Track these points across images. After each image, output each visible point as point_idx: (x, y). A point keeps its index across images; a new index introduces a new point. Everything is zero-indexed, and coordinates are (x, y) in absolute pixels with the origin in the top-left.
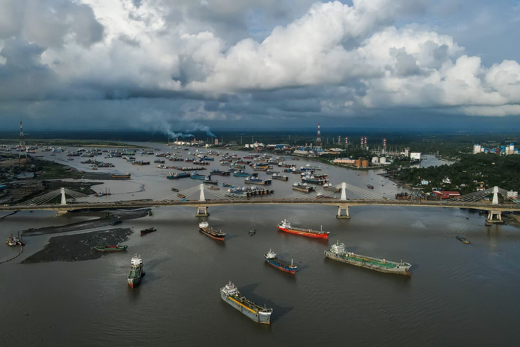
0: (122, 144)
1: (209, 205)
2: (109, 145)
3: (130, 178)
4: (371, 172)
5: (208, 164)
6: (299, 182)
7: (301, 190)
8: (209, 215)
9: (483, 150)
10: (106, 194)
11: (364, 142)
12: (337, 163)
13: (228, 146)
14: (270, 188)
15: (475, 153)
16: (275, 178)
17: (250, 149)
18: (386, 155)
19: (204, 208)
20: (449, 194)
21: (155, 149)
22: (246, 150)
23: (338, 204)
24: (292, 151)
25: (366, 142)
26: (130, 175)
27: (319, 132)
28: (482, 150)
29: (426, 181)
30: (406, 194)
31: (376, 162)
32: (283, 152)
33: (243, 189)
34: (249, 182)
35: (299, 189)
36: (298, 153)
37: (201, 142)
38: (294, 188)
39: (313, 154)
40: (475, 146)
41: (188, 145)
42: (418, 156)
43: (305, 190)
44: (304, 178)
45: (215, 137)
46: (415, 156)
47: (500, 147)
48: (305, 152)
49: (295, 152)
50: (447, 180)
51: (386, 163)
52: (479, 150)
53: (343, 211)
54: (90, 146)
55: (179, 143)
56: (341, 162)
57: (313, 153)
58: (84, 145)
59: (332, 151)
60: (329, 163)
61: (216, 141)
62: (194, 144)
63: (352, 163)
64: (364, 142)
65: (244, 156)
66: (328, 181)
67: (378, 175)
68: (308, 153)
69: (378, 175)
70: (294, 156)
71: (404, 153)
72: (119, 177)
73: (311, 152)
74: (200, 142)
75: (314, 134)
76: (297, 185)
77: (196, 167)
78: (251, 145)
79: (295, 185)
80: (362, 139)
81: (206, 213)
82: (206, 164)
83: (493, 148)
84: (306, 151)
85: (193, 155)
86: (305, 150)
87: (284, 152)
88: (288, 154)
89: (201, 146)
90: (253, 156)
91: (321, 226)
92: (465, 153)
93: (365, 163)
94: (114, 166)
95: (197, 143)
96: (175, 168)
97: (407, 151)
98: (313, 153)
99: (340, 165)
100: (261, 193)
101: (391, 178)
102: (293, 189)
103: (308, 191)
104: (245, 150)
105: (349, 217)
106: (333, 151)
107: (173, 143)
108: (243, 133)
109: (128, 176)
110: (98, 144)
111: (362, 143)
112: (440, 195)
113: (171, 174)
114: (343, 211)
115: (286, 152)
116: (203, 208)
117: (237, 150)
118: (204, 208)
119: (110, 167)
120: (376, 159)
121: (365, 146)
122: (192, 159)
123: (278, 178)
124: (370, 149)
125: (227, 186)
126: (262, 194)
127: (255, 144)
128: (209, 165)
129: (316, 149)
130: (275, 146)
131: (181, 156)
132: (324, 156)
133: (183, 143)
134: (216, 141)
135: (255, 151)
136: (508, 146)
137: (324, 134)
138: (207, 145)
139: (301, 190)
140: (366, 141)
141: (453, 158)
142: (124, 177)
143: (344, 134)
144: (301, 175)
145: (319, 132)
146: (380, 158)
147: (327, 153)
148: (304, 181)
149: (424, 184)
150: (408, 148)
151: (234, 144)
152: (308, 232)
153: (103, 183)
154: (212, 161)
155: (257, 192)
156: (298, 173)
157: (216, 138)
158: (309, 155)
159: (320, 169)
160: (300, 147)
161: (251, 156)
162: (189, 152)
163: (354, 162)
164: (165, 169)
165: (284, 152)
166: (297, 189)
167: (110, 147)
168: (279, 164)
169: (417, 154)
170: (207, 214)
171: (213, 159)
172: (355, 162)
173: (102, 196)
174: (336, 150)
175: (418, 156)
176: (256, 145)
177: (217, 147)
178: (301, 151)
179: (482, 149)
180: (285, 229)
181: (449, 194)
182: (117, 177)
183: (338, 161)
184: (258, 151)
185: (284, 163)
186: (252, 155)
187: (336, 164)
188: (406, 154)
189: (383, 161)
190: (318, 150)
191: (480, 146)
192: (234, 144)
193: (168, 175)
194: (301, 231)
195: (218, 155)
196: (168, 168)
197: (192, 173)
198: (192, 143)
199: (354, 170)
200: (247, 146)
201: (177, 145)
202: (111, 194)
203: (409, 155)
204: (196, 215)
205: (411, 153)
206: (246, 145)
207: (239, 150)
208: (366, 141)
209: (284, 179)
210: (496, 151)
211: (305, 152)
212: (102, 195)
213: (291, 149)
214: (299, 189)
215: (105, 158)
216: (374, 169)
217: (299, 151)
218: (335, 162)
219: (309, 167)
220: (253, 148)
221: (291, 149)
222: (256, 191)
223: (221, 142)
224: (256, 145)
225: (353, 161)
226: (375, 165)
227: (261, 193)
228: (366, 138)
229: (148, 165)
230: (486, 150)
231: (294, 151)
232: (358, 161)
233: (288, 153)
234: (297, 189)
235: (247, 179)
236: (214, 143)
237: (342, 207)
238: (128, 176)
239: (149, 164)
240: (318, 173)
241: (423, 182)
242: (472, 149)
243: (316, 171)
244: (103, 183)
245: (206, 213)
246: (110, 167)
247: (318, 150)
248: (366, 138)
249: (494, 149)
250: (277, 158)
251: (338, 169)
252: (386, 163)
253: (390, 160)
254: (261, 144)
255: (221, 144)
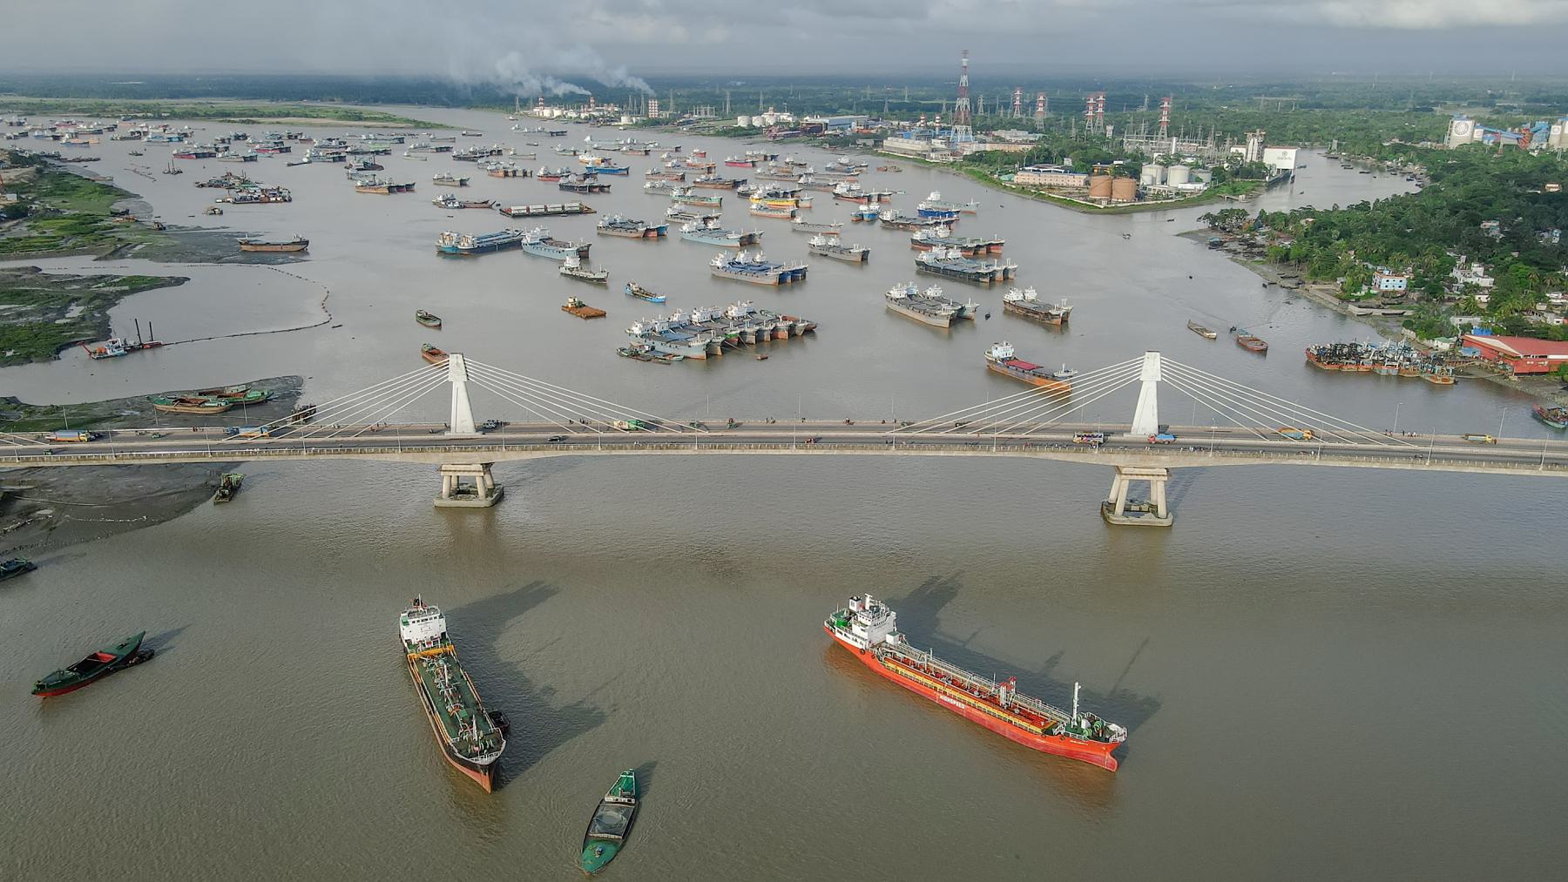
0: (378, 113)
1: (497, 457)
2: (340, 118)
3: (308, 254)
4: (1142, 224)
5: (606, 189)
6: (911, 283)
7: (917, 316)
8: (500, 498)
9: (1478, 134)
10: (141, 344)
11: (1095, 109)
12: (1029, 184)
13: (688, 122)
14: (797, 306)
15: (1453, 146)
16: (823, 254)
17: (750, 132)
18: (1185, 157)
19: (473, 467)
20: (1550, 357)
21: (464, 132)
22: (739, 135)
23: (1117, 459)
24: (878, 140)
25: (1100, 110)
26: (307, 243)
27: (964, 79)
28: (1475, 136)
29: (1398, 279)
30: (1354, 353)
31: (1154, 179)
32: (849, 142)
33: (695, 318)
34: (727, 275)
35: (910, 313)
36: (895, 148)
37: (610, 109)
38: (894, 306)
39: (942, 150)
40: (1456, 122)
41: (571, 117)
42: (1289, 158)
43: (933, 321)
44: (925, 257)
45: (651, 92)
46: (1279, 158)
47: (1533, 125)
48: (919, 146)
49: (886, 143)
50: (1474, 269)
51: (1189, 186)
52: (1468, 134)
53: (1139, 489)
54: (278, 123)
55: (547, 113)
56: (1037, 183)
57: (943, 146)
58: (261, 120)
59: (1001, 140)
60: (998, 184)
61: (653, 106)
62: (587, 115)
63: (1077, 184)
64: (1095, 109)
65: (729, 159)
66: (1015, 270)
67: (1178, 235)
68: (927, 148)
69: (1178, 235)
70: (885, 155)
71: (1242, 150)
72: (264, 248)
73: (937, 143)
74: (607, 111)
75: (954, 92)
76: (903, 296)
77: (560, 205)
78: (754, 118)
79: (895, 293)
80: (1092, 101)
81: (481, 492)
82: (597, 190)
83: (1510, 129)
84: (922, 143)
85: (572, 153)
86: (918, 138)
87: (854, 143)
88: (866, 150)
89: (609, 121)
90: (756, 156)
91: (1077, 687)
92: (1409, 144)
93: (1124, 186)
94: (290, 200)
95: (595, 114)
96: (490, 207)
97: (1253, 143)
98: (943, 146)
99: (1039, 194)
100: (767, 337)
101: (1235, 252)
102: (889, 312)
103: (946, 323)
104: (735, 136)
105: (1167, 523)
106: (1009, 142)
107: (529, 112)
108: (739, 81)
109: (300, 247)
110: (306, 116)
111: (1091, 113)
112: (1508, 357)
113: (451, 241)
114: (1139, 489)
115: (858, 143)
116: (467, 466)
117: (712, 135)
118: (473, 467)
119: (273, 202)
120: (1154, 170)
121: (1097, 122)
122: (559, 171)
123: (830, 254)
124: (1118, 132)
125: (640, 297)
126: (766, 342)
127: (765, 115)
128: (609, 192)
129: (953, 132)
130: (827, 121)
131: (533, 157)
132: (978, 158)
133: (557, 113)
134: (653, 106)
135: (765, 139)
136: (1559, 121)
137: (972, 91)
138: (624, 120)
139: (917, 316)
140: (1165, 112)
141: (1389, 163)
142: (285, 249)
143: (1032, 86)
144: (912, 240)
145: (964, 79)
146: (1170, 168)
147: (988, 147)
148: (926, 270)
149: (1390, 288)
150: (1258, 133)
151: (706, 114)
152: (993, 700)
153: (179, 281)
154: (623, 178)
155: (750, 334)
156: (899, 229)
157: (652, 98)
158: (933, 155)
159: (973, 210)
160: (902, 123)
161: (751, 157)
162: (559, 145)
163: (1082, 184)
164: (456, 210)
165: (854, 143)
166: (903, 310)
167: (336, 126)
168: (838, 190)
169: (1285, 154)
170: (489, 492)
171: (627, 169)
172: (1087, 183)
173: (122, 355)
174: (1017, 141)
175: (1289, 158)
176: (769, 118)
177: (655, 123)
178: (906, 140)
179: (1476, 130)
180: (863, 652)
181: (1550, 357)
182: (259, 249)
183: (1026, 177)
184: (776, 140)
185: (854, 187)
186: (755, 153)
187: (1023, 190)
188: (1250, 152)
189: (1178, 178)
190: (961, 138)
191: (1470, 123)
192: (706, 114)
193: (441, 241)
194: (954, 682)
195: (647, 152)
196: (465, 207)
197: (531, 232)
198: (584, 112)
199: (1091, 213)
200: (742, 121)
201: (539, 117)
202: (159, 345)
203: (1260, 155)
204: (437, 503)
205: (1266, 150)
206: (739, 118)
207: (718, 134)
208: (1041, 104)
209: (853, 259)
210: (1517, 139)
211: (919, 146)
212: (122, 351)
213: (872, 131)
214: (910, 313)
215: (289, 165)
216: (1154, 209)
217: (900, 140)
218: (1019, 181)
219: (937, 202)
220: (761, 128)
221: (872, 131)
222: (747, 330)
223: (668, 110)
224: (769, 118)
225: (1078, 180)
226: (1157, 196)
227: (767, 337)
228: (1101, 98)
229: (408, 194)
230: (1489, 135)
231: (885, 141)
232: (1099, 182)
233: (864, 144)
234: (903, 310)
235: (719, 264)
236: (647, 114)
237: (1137, 471)
238: (300, 247)
239: (413, 191)
240: (973, 232)
241: (1384, 280)
242: (1442, 132)
243: (964, 220)
244: (179, 281)
245: (481, 492)
246: (273, 202)
247: (959, 137)
248: (1101, 98)
249: (1512, 131)
250: (828, 166)
251: (1032, 206)
252: (1189, 186)
253: (1201, 176)
254: (786, 117)
255: (665, 115)
